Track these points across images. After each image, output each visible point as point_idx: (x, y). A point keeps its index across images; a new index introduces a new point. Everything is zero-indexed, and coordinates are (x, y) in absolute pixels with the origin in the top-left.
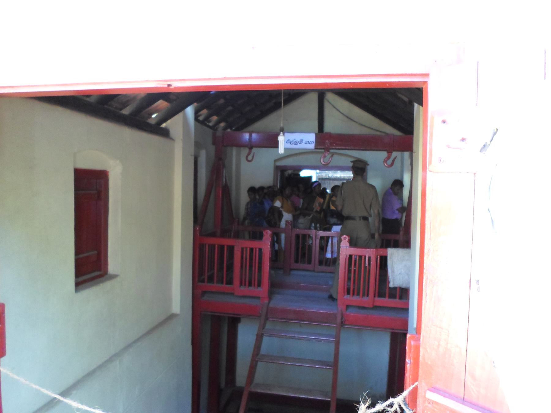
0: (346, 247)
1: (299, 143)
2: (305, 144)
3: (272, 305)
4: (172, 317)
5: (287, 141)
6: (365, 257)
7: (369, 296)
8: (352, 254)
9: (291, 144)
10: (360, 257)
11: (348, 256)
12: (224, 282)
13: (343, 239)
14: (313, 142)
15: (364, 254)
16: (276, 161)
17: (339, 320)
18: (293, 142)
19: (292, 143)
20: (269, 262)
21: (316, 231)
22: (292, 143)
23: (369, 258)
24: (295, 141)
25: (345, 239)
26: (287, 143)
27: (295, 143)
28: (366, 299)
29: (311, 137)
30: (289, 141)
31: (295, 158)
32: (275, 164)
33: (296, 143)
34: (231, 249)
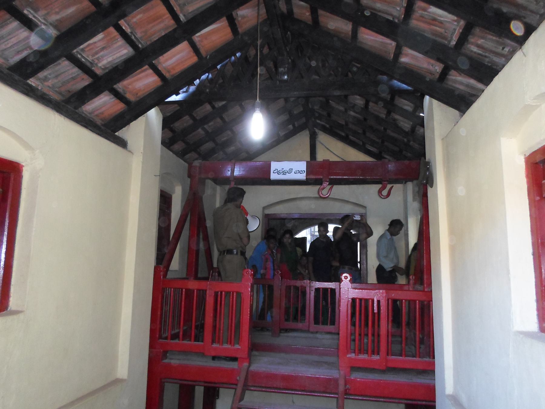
0: (348, 289)
1: (288, 173)
2: (295, 173)
3: (254, 368)
4: (117, 381)
5: (274, 171)
6: (373, 300)
7: (380, 353)
8: (355, 297)
9: (278, 174)
10: (366, 300)
11: (355, 285)
12: (193, 338)
13: (343, 278)
14: (304, 171)
15: (372, 298)
16: (264, 208)
17: (341, 388)
18: (280, 172)
19: (280, 173)
20: (134, 74)
21: (310, 282)
22: (280, 173)
23: (379, 302)
24: (283, 170)
25: (346, 278)
26: (273, 172)
27: (283, 173)
28: (376, 357)
29: (302, 166)
30: (277, 171)
31: (286, 205)
32: (263, 211)
33: (284, 173)
34: (202, 293)
